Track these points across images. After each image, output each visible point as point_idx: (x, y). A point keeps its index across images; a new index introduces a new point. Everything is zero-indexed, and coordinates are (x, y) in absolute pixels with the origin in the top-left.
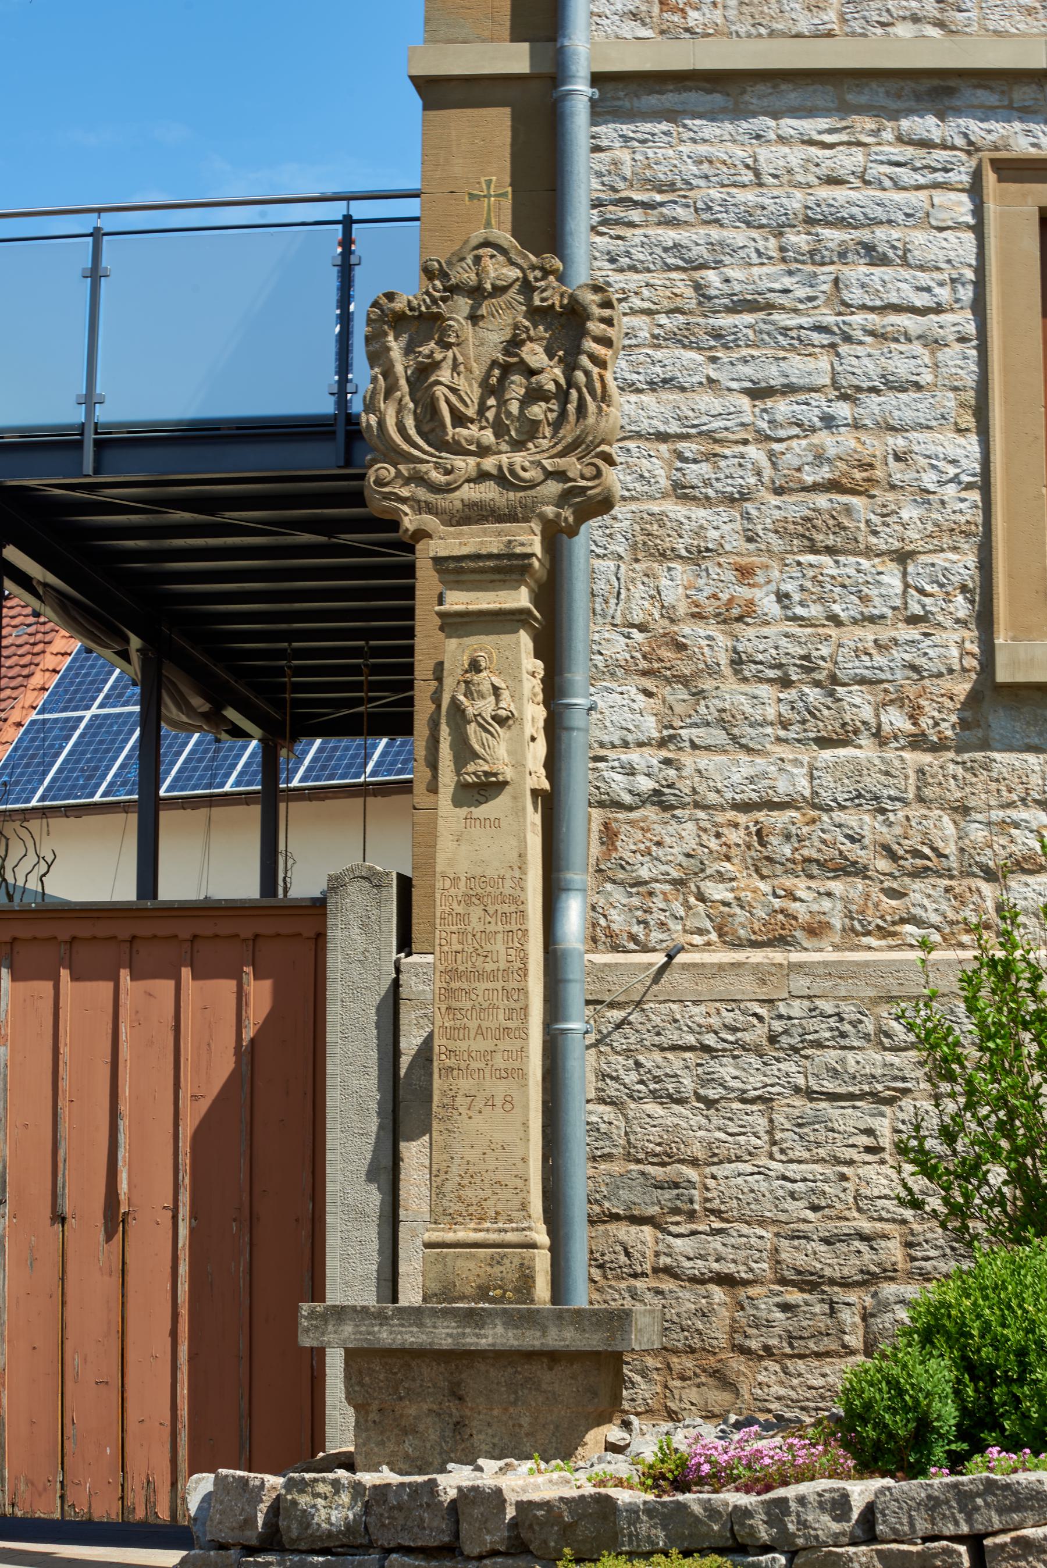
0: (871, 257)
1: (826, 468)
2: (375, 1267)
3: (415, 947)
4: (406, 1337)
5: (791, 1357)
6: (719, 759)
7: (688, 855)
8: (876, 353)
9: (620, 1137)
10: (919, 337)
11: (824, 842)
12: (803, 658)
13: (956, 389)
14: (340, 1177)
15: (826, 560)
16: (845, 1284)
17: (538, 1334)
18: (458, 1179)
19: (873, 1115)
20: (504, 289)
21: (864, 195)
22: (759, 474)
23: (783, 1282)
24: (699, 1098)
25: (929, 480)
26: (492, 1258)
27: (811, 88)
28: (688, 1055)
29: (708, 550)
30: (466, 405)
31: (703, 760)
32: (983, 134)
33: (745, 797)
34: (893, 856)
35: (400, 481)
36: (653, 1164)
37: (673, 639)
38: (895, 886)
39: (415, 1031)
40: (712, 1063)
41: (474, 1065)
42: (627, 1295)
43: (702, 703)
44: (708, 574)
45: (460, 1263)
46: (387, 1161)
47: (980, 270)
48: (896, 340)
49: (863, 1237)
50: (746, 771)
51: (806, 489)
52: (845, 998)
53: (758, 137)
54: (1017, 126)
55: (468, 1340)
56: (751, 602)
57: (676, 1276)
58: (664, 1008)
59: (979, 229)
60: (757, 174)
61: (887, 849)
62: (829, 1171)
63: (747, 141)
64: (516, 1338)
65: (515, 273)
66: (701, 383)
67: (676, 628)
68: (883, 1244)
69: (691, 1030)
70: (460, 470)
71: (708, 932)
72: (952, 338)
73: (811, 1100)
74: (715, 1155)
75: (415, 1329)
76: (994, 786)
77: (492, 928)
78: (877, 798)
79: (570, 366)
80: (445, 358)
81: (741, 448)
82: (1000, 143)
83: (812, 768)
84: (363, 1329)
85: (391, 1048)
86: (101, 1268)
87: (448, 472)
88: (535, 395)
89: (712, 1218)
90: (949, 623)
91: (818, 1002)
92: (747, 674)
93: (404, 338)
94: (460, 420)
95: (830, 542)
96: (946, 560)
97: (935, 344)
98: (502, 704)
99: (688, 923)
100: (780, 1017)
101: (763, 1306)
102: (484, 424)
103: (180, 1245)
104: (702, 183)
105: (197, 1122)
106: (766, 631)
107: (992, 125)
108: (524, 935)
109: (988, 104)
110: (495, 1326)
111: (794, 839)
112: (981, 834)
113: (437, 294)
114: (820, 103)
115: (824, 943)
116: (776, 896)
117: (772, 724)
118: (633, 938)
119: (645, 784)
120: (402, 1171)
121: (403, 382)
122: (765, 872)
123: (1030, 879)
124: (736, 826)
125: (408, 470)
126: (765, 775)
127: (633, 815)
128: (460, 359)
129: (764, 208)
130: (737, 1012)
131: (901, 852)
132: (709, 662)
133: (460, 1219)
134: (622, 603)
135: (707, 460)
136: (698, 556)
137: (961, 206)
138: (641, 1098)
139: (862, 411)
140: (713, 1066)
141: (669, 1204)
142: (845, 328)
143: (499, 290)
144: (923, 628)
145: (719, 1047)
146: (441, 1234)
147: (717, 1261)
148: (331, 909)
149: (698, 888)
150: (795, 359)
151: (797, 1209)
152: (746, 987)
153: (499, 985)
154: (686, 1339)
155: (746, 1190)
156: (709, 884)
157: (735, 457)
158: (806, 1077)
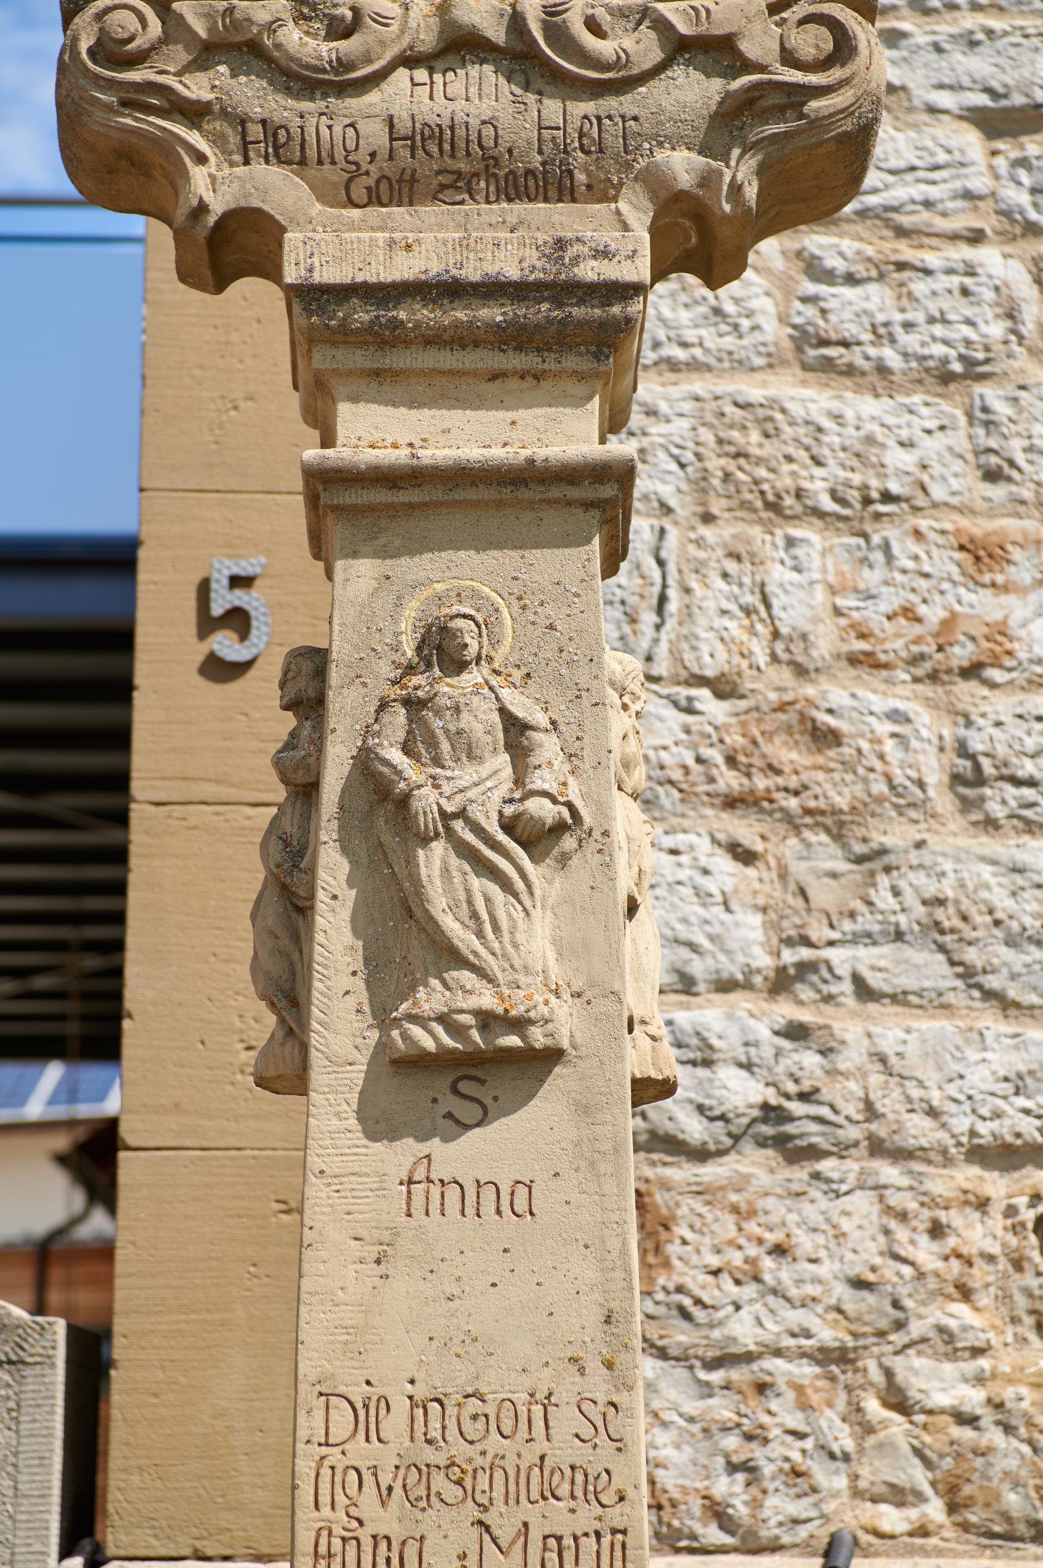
7: (859, 1284)
29: (887, 497)
33: (1003, 1128)
35: (180, 56)
37: (803, 717)
43: (884, 881)
44: (889, 557)
56: (1001, 631)
67: (810, 691)
70: (381, 20)
71: (920, 1497)
81: (965, 252)
98: (539, 781)
99: (865, 1472)
124: (982, 1205)
127: (710, 1172)
132: (899, 778)
134: (670, 624)
135: (881, 277)
149: (889, 1373)
157: (950, 271)
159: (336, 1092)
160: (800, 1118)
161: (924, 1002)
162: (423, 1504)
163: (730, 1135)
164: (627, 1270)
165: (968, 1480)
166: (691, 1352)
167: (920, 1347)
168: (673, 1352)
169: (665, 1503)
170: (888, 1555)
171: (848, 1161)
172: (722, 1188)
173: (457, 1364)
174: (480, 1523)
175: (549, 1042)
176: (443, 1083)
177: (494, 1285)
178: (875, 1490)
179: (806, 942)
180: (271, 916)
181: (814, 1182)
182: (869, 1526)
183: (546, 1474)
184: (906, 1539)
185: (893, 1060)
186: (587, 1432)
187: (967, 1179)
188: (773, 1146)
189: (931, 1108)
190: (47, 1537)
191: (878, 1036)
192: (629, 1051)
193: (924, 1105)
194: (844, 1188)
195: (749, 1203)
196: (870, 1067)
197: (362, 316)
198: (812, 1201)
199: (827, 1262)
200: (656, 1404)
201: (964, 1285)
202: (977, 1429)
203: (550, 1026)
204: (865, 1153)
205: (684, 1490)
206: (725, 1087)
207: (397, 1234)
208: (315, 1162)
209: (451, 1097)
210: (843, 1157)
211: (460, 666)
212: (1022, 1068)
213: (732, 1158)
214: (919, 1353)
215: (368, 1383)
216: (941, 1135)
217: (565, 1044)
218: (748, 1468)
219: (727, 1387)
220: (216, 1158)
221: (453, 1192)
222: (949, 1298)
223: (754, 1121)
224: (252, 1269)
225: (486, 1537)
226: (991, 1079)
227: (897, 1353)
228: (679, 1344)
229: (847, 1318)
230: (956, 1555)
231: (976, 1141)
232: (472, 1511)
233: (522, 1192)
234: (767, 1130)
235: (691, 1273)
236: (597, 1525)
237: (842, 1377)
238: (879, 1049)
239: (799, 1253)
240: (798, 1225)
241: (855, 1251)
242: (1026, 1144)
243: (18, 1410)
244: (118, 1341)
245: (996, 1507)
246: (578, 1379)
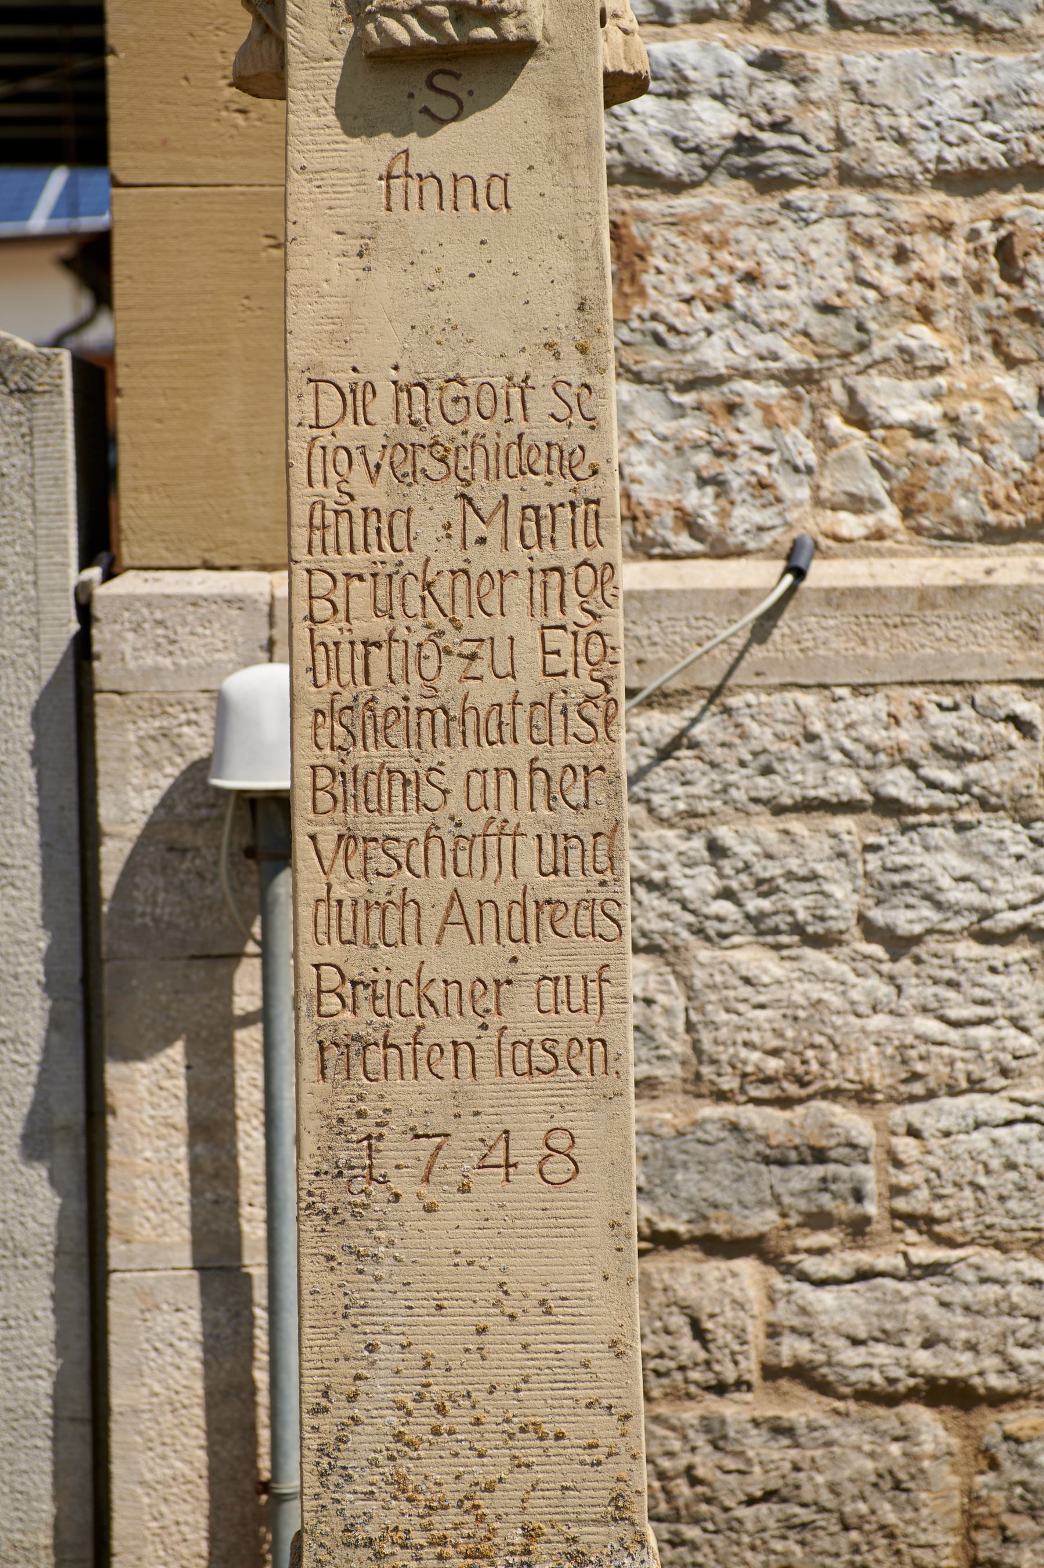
2: (46, 1386)
3: (128, 551)
6: (902, 52)
7: (825, 308)
9: (672, 1033)
18: (394, 1418)
24: (870, 931)
28: (843, 823)
33: (969, 154)
36: (758, 1102)
39: (137, 776)
40: (903, 841)
42: (700, 1440)
57: (823, 1388)
58: (781, 704)
69: (852, 760)
71: (877, 504)
74: (915, 1077)
77: (489, 558)
85: (72, 816)
89: (911, 1235)
99: (827, 484)
108: (600, 583)
118: (689, 522)
122: (1017, 348)
124: (946, 230)
127: (684, 203)
130: (967, 711)
138: (724, 936)
141: (802, 1204)
145: (923, 802)
147: (927, 1345)
149: (851, 392)
154: (856, 1549)
155: (995, 1164)
156: (880, 381)
159: (314, 88)
160: (771, 149)
161: (896, 28)
162: (409, 479)
163: (704, 166)
164: (600, 260)
165: (923, 488)
166: (665, 376)
167: (882, 367)
168: (648, 376)
169: (639, 514)
170: (845, 556)
171: (818, 190)
172: (696, 219)
173: (438, 351)
174: (463, 496)
175: (522, 33)
177: (472, 275)
178: (836, 499)
181: (785, 212)
182: (829, 530)
183: (524, 451)
184: (864, 543)
185: (865, 88)
186: (562, 412)
187: (933, 205)
188: (746, 178)
189: (901, 135)
190: (66, 549)
191: (851, 64)
192: (602, 44)
193: (894, 133)
194: (813, 216)
195: (722, 233)
196: (842, 95)
198: (782, 230)
199: (795, 288)
200: (631, 425)
201: (926, 307)
202: (933, 441)
203: (523, 17)
204: (835, 181)
205: (658, 503)
206: (701, 120)
207: (378, 228)
208: (296, 158)
209: (427, 91)
210: (812, 186)
212: (991, 93)
213: (705, 190)
214: (881, 373)
215: (354, 369)
216: (910, 163)
217: (538, 36)
218: (719, 483)
219: (699, 407)
220: (205, 195)
221: (431, 186)
222: (913, 320)
223: (728, 152)
224: (245, 302)
225: (469, 509)
226: (960, 104)
227: (859, 373)
228: (653, 368)
229: (813, 341)
230: (908, 555)
231: (943, 167)
232: (454, 485)
233: (497, 185)
234: (740, 161)
235: (665, 301)
236: (572, 496)
237: (807, 397)
238: (852, 77)
239: (769, 280)
240: (768, 253)
241: (822, 278)
242: (992, 169)
243: (31, 433)
244: (121, 371)
245: (947, 511)
246: (553, 363)
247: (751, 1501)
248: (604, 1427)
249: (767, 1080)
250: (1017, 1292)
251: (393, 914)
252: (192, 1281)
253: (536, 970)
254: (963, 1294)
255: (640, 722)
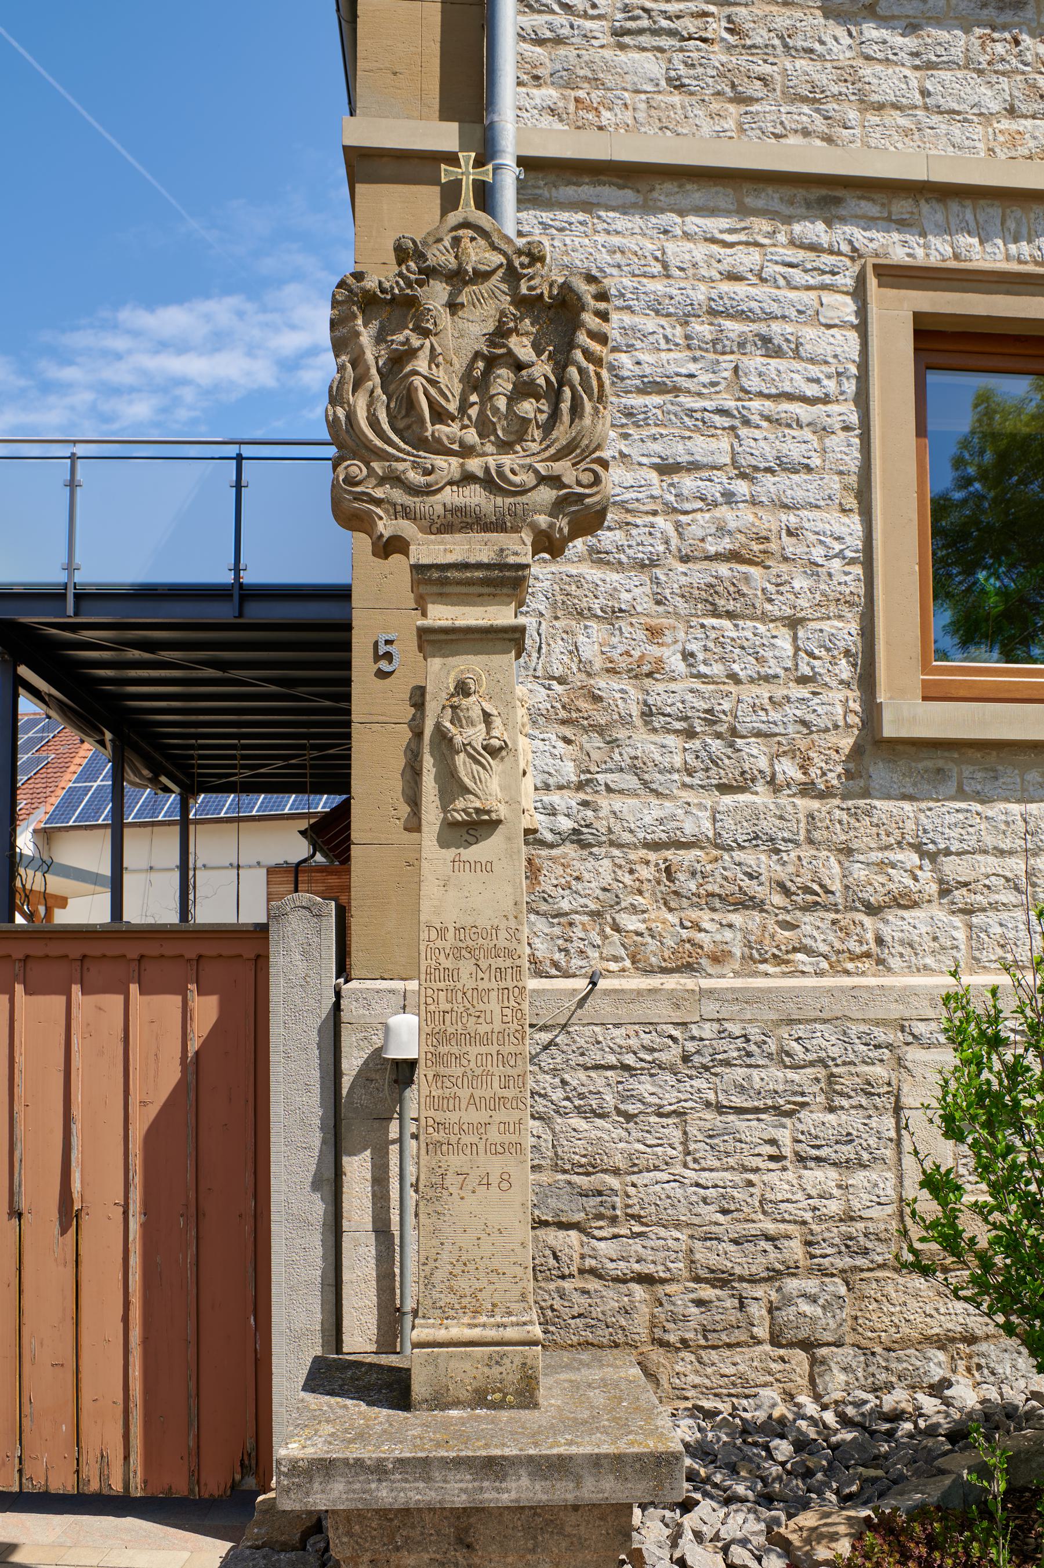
0: (767, 349)
1: (727, 540)
2: (319, 1273)
3: (354, 973)
4: (411, 1494)
5: (706, 1347)
6: (632, 801)
7: (604, 890)
8: (772, 437)
10: (809, 425)
11: (726, 879)
12: (706, 711)
13: (841, 473)
14: (284, 1188)
15: (726, 623)
16: (753, 1280)
17: (571, 1485)
18: (450, 1267)
19: (775, 1127)
20: (486, 275)
21: (761, 291)
22: (667, 542)
23: (697, 1279)
24: (619, 1112)
25: (817, 554)
26: (490, 1358)
27: (714, 190)
28: (609, 1073)
29: (621, 610)
30: (447, 400)
31: (618, 803)
32: (866, 242)
33: (656, 837)
34: (786, 892)
35: (373, 481)
38: (788, 918)
39: (356, 1053)
41: (466, 1139)
42: (556, 1295)
43: (617, 750)
44: (621, 633)
45: (453, 1364)
46: (329, 1174)
47: (864, 366)
48: (789, 426)
49: (768, 1238)
50: (657, 813)
51: (708, 558)
52: (750, 1021)
53: (666, 232)
54: (896, 236)
55: (486, 1496)
56: (660, 660)
57: (600, 1277)
58: (587, 1031)
59: (862, 328)
60: (665, 266)
61: (782, 885)
62: (738, 1178)
63: (656, 235)
64: (544, 1491)
65: (498, 259)
66: (614, 457)
67: (592, 682)
68: (786, 1243)
70: (441, 469)
71: (623, 959)
72: (838, 426)
73: (721, 1114)
74: (635, 1165)
75: (421, 1485)
76: (874, 830)
78: (772, 840)
79: (561, 365)
80: (422, 346)
81: (651, 519)
82: (880, 251)
83: (715, 812)
84: (357, 1486)
85: (332, 1067)
86: (56, 1260)
87: (428, 472)
88: (524, 390)
89: (633, 1222)
90: (834, 684)
91: (727, 1025)
92: (657, 725)
93: (375, 324)
94: (440, 415)
95: (731, 608)
96: (832, 627)
97: (825, 431)
98: (494, 733)
100: (693, 1038)
101: (680, 1302)
102: (466, 422)
103: (131, 1239)
104: (615, 271)
105: (146, 1127)
106: (673, 686)
107: (873, 234)
109: (870, 214)
110: (519, 1477)
111: (699, 875)
112: (862, 873)
113: (412, 276)
114: (722, 205)
115: (726, 970)
116: (684, 927)
117: (678, 771)
118: (555, 965)
119: (566, 824)
120: (345, 1185)
121: (374, 371)
122: (673, 905)
123: (906, 914)
125: (383, 468)
126: (673, 817)
127: (554, 852)
128: (439, 350)
129: (672, 298)
131: (793, 889)
133: (452, 1313)
136: (613, 615)
137: (845, 308)
139: (759, 489)
140: (632, 1083)
142: (745, 412)
143: (482, 276)
144: (811, 687)
146: (431, 1331)
147: (638, 1262)
148: (273, 936)
149: (614, 919)
150: (699, 439)
151: (709, 1212)
152: (662, 1012)
153: (493, 1049)
154: (611, 1335)
158: (716, 1093)
176: (464, 830)
179: (590, 772)
180: (408, 776)
197: (436, 575)
208: (424, 855)
211: (469, 695)
218: (566, 951)
232: (474, 961)
247: (574, 1317)
248: (519, 1271)
249: (581, 1166)
250: (670, 1242)
251: (451, 1101)
252: (373, 1236)
253: (498, 1120)
254: (651, 1243)
255: (537, 1036)
